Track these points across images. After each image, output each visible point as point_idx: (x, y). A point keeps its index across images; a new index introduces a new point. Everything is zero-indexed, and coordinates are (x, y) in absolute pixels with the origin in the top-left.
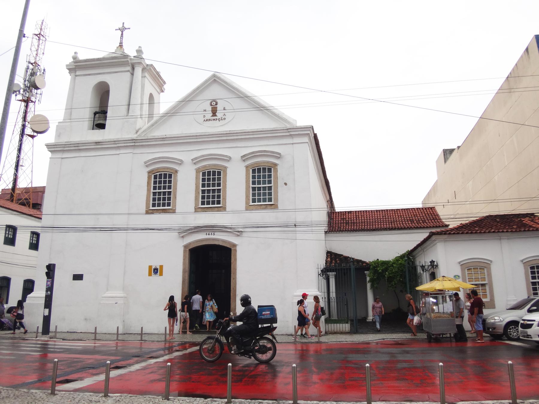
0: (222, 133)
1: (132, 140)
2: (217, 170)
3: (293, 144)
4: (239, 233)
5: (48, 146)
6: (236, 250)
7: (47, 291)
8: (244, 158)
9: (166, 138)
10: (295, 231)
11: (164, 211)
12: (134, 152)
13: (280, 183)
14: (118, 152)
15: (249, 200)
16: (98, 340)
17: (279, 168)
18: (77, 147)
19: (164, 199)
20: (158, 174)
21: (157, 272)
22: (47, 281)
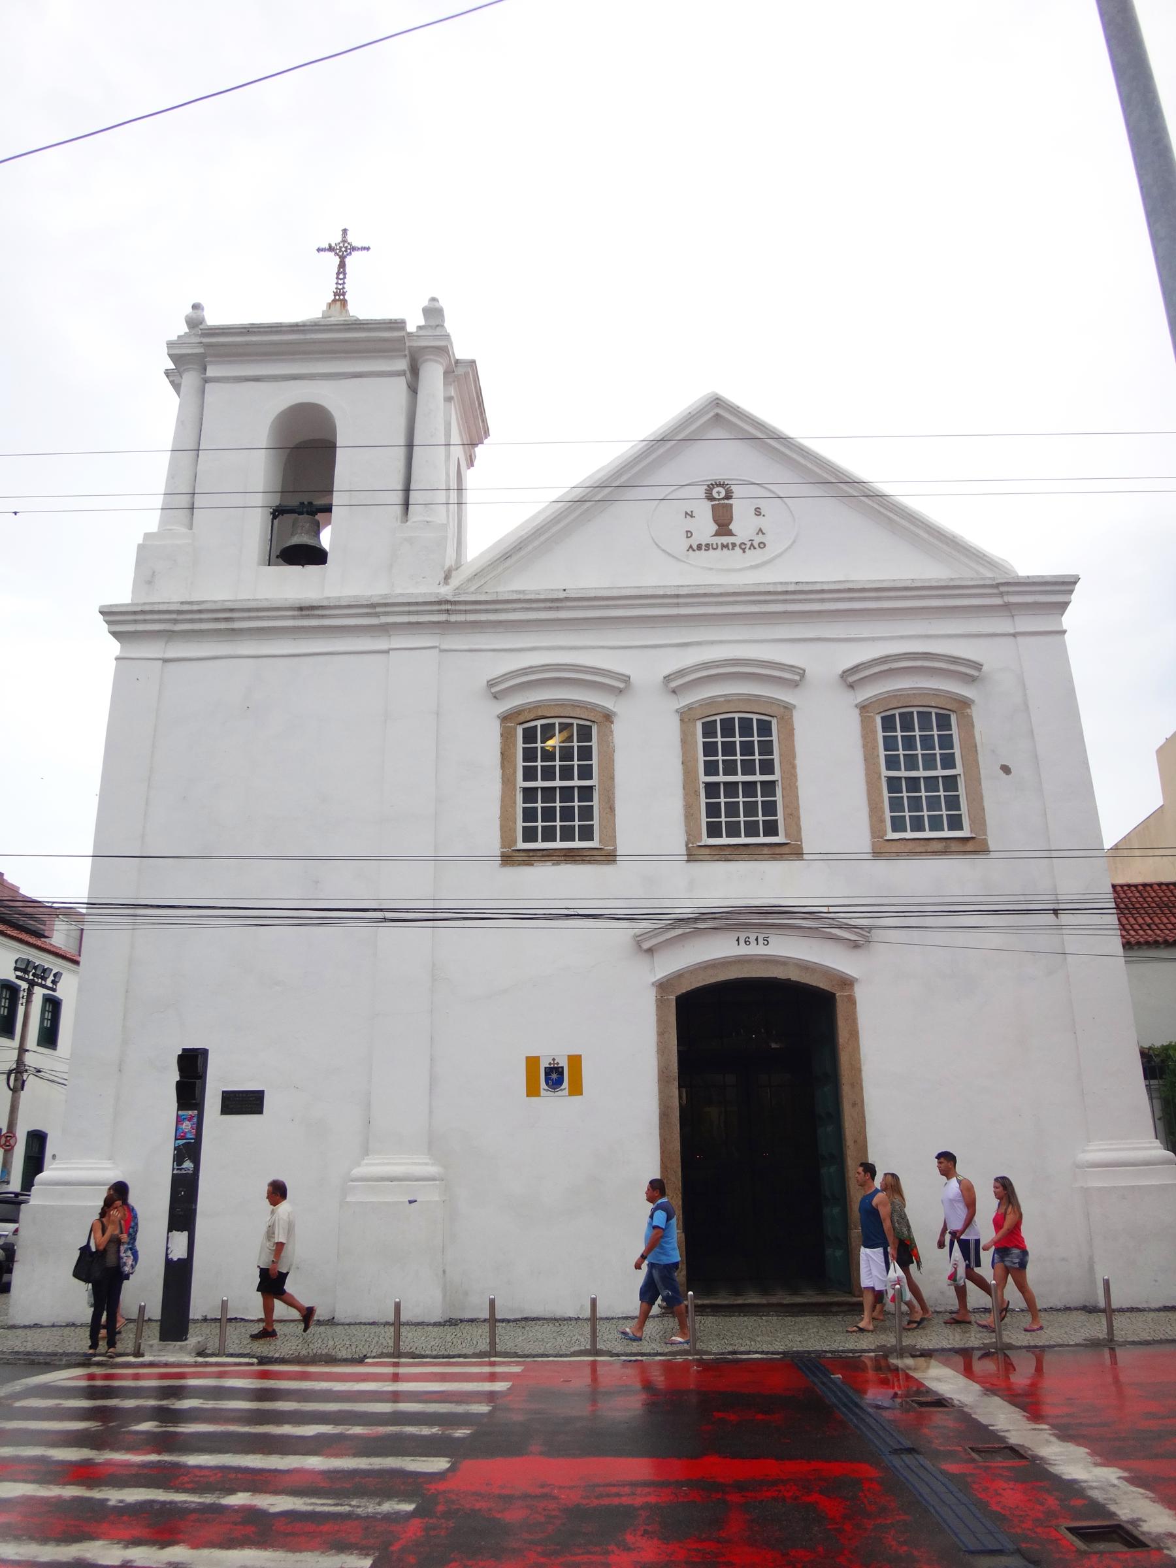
0: (771, 589)
1: (440, 603)
2: (755, 717)
3: (1014, 635)
4: (859, 939)
5: (110, 614)
6: (852, 1001)
7: (179, 1158)
8: (851, 678)
9: (567, 599)
10: (1059, 927)
11: (571, 856)
12: (444, 647)
13: (987, 766)
14: (381, 644)
15: (883, 821)
16: (506, 1354)
17: (976, 713)
18: (227, 623)
19: (567, 814)
20: (539, 723)
21: (559, 1082)
22: (179, 1120)
